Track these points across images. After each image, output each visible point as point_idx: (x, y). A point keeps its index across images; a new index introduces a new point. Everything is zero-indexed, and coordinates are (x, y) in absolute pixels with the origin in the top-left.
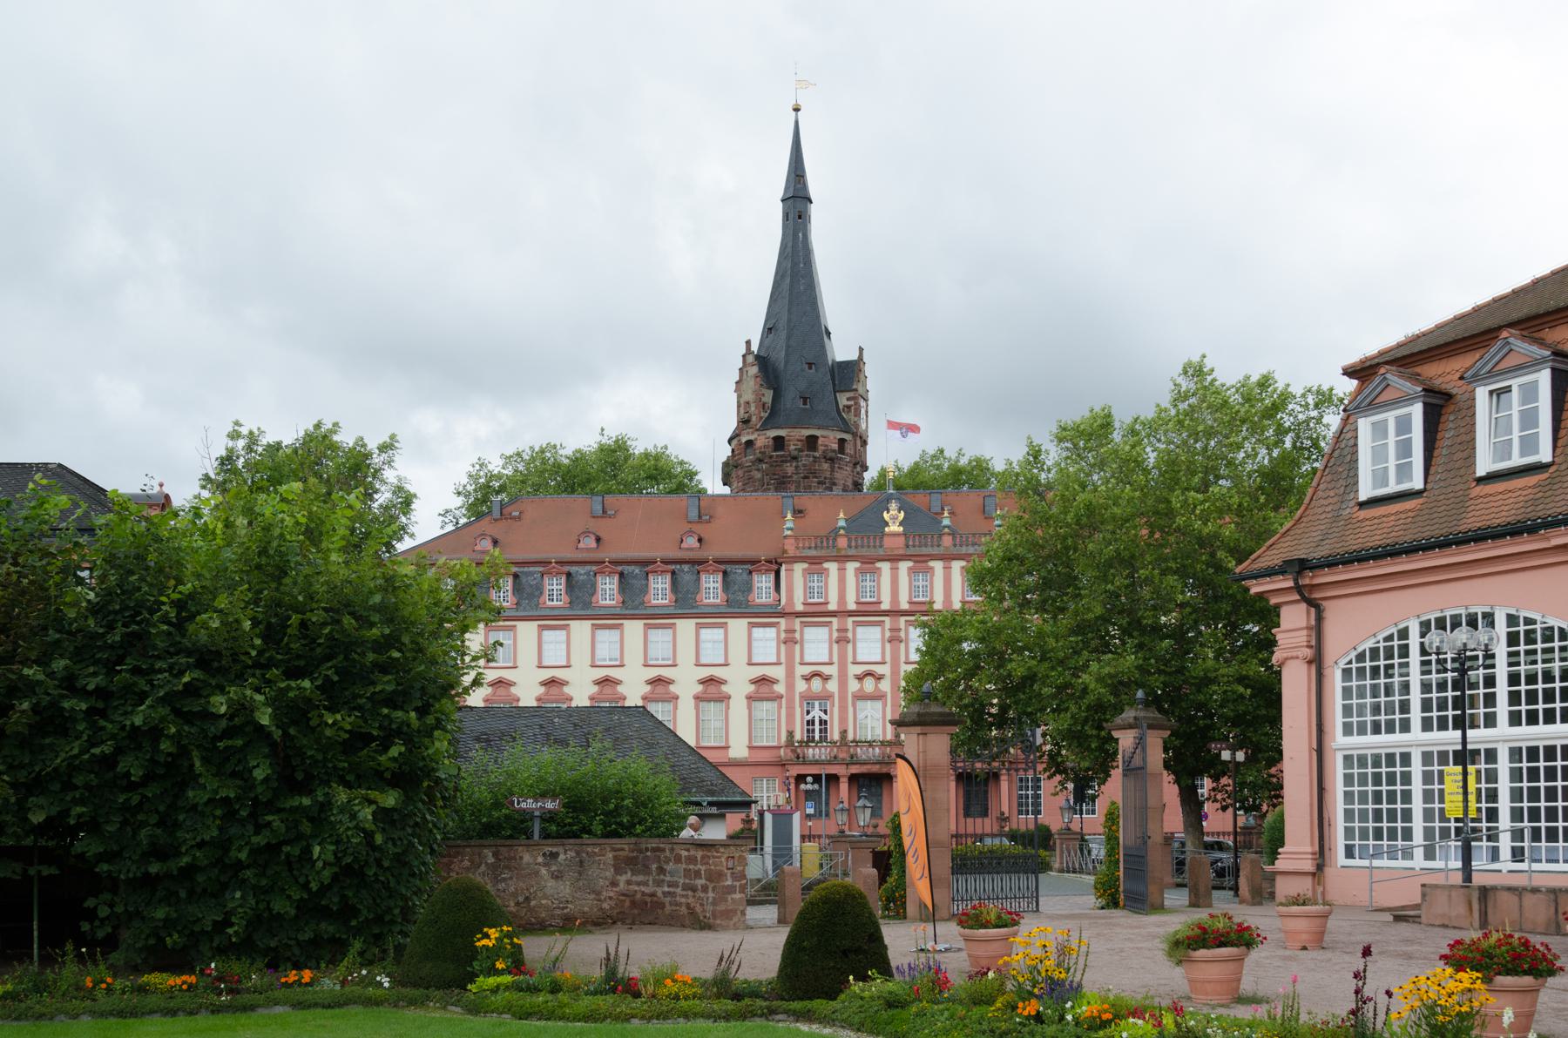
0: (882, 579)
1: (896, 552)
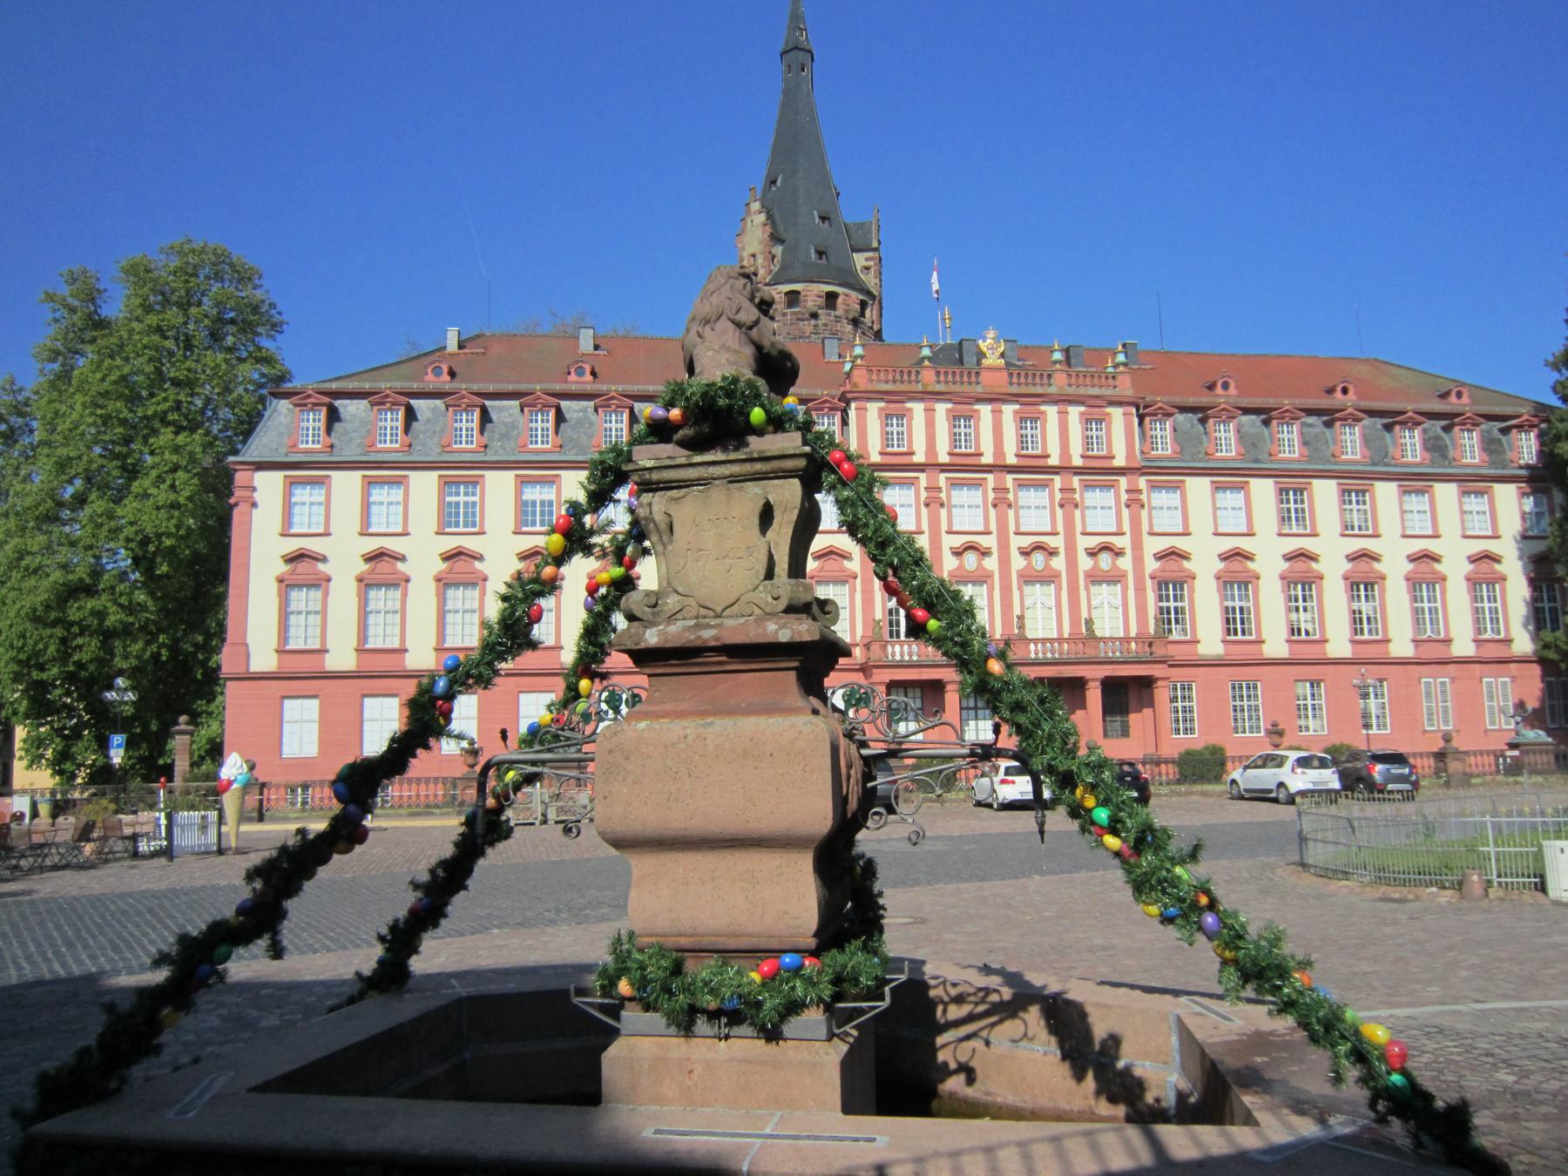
0: (1048, 426)
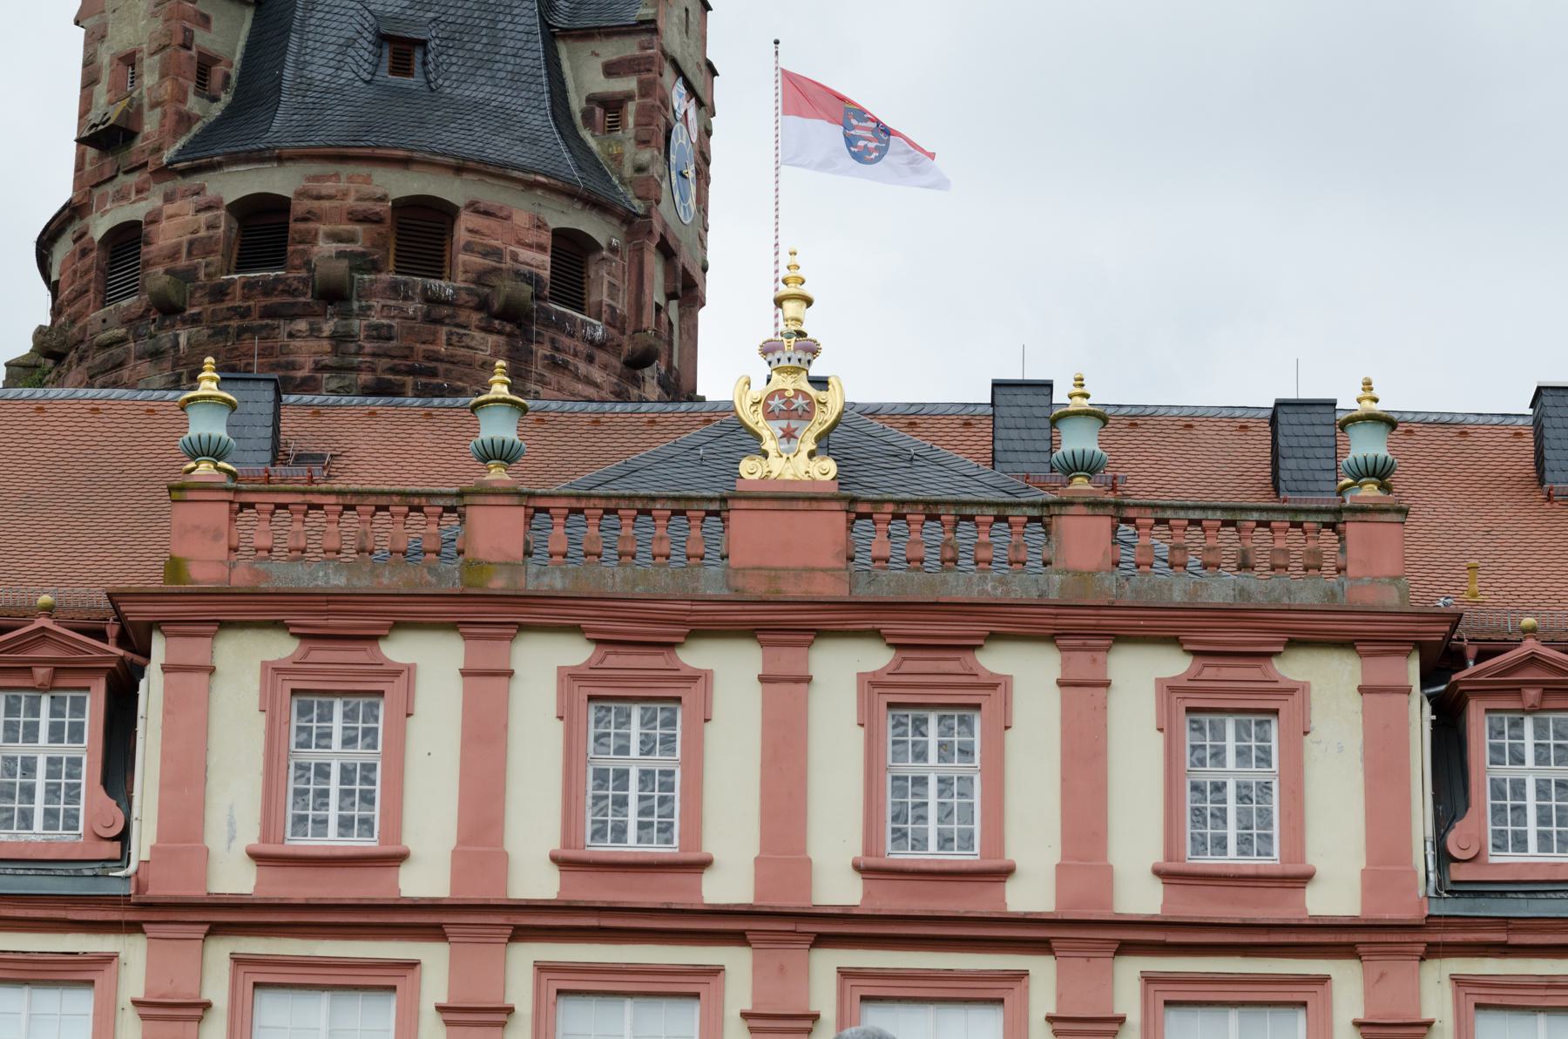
1: (793, 590)
